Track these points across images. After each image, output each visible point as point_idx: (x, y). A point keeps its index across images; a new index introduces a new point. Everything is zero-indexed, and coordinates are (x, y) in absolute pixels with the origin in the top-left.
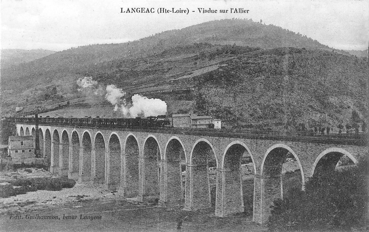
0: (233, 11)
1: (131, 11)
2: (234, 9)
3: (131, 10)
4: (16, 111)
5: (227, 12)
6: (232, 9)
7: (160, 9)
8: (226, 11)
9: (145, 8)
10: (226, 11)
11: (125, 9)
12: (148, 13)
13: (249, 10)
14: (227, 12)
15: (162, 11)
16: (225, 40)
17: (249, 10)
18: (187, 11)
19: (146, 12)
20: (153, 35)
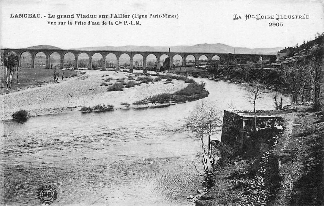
0: (113, 16)
1: (19, 16)
2: (114, 15)
3: (18, 16)
4: (186, 64)
5: (64, 24)
6: (112, 15)
7: (134, 15)
8: (63, 23)
9: (289, 16)
10: (63, 23)
11: (14, 15)
12: (17, 18)
13: (108, 15)
14: (64, 24)
15: (122, 17)
16: (75, 129)
17: (108, 15)
18: (177, 17)
19: (15, 17)
20: (286, 48)
